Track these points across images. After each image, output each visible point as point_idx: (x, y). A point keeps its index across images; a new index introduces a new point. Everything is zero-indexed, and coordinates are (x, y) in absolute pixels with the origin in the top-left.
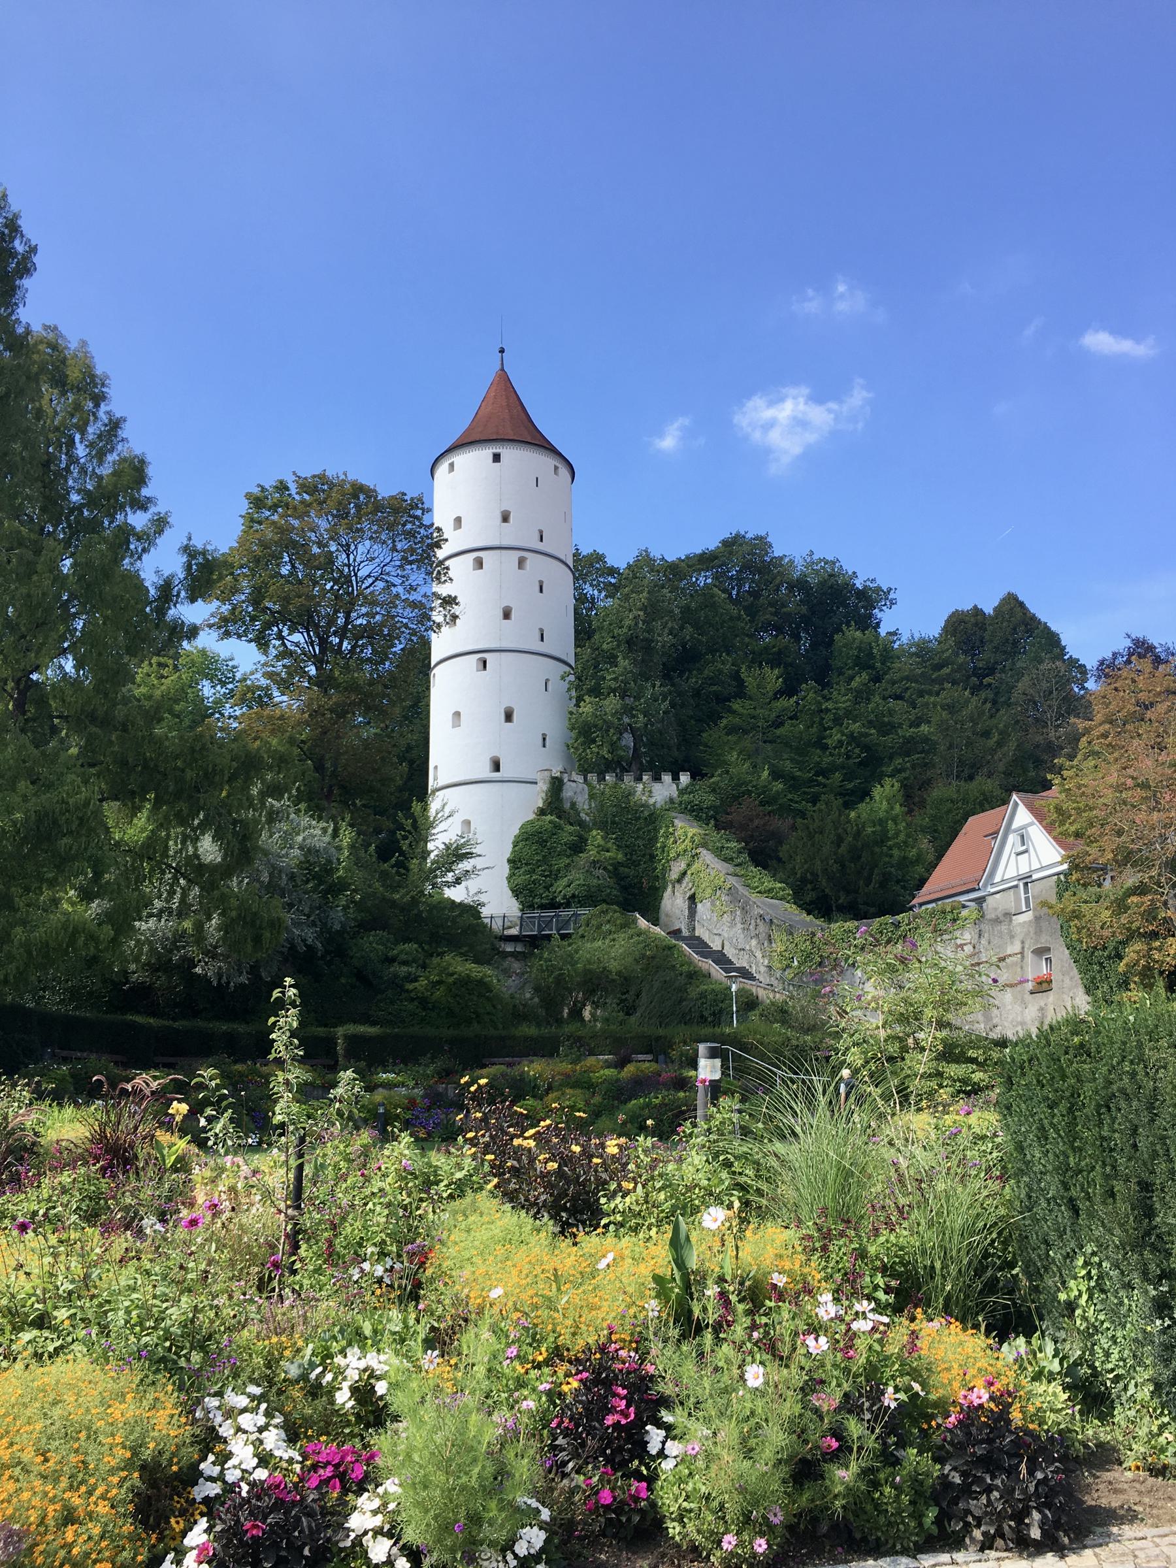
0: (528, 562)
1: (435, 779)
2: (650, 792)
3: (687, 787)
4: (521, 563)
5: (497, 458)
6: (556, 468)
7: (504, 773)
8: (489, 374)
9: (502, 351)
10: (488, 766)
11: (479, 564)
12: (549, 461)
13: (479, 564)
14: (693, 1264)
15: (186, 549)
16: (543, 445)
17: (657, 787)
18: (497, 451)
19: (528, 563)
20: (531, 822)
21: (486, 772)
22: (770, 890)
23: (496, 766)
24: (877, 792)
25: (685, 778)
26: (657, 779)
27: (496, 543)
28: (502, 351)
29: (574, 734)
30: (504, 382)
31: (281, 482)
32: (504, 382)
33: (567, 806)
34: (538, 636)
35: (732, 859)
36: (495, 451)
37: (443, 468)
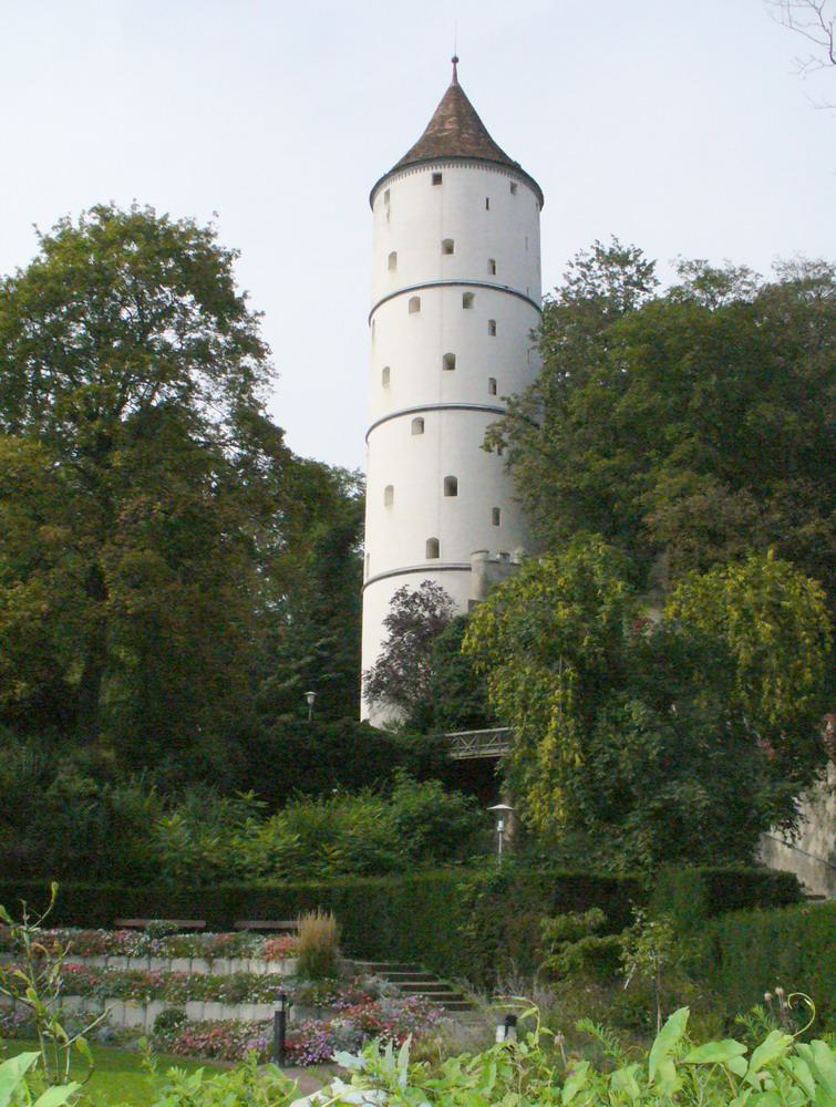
0: (475, 299)
1: (368, 574)
4: (467, 302)
5: (437, 179)
6: (513, 188)
7: (446, 557)
8: (449, 82)
9: (455, 60)
10: (423, 549)
11: (416, 305)
12: (502, 180)
13: (416, 305)
16: (497, 160)
18: (438, 170)
19: (475, 302)
20: (327, 467)
21: (422, 560)
23: (434, 548)
28: (455, 60)
29: (93, 220)
30: (456, 96)
31: (669, 262)
32: (456, 96)
34: (486, 327)
37: (380, 196)
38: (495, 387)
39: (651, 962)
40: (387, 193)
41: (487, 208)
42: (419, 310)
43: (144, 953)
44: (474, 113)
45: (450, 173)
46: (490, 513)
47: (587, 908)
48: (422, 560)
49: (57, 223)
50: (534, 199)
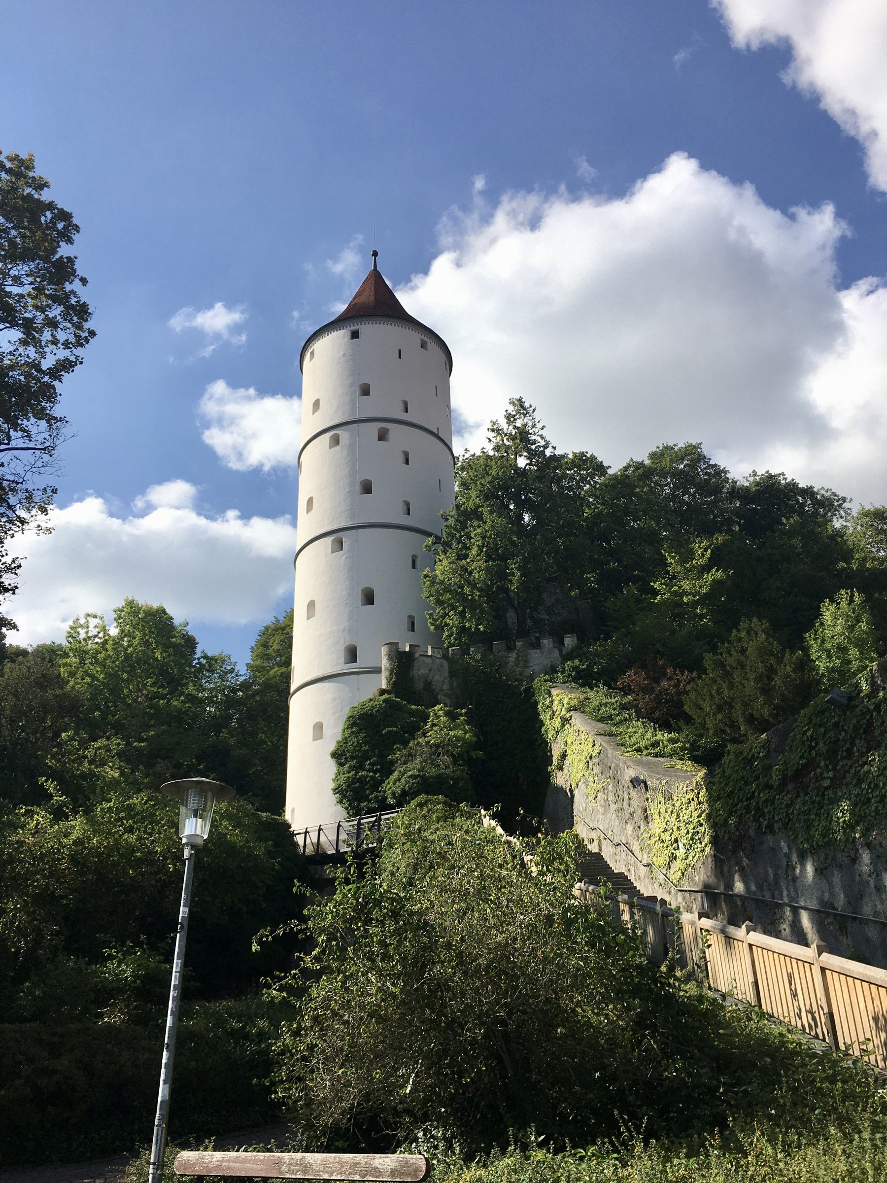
2: (526, 661)
3: (573, 650)
5: (355, 335)
6: (423, 345)
9: (375, 254)
10: (341, 656)
13: (336, 441)
14: (456, 455)
15: (76, 258)
17: (535, 654)
18: (356, 327)
21: (340, 666)
22: (655, 744)
23: (352, 654)
24: (828, 612)
25: (569, 641)
26: (537, 645)
27: (349, 524)
28: (375, 254)
30: (376, 278)
32: (376, 278)
33: (419, 686)
34: (401, 458)
35: (610, 718)
36: (353, 328)
38: (409, 509)
39: (876, 808)
40: (312, 353)
41: (400, 357)
42: (338, 444)
43: (61, 299)
44: (292, 637)
45: (368, 329)
46: (405, 620)
47: (819, 614)
48: (340, 666)
49: (24, 156)
50: (444, 358)
